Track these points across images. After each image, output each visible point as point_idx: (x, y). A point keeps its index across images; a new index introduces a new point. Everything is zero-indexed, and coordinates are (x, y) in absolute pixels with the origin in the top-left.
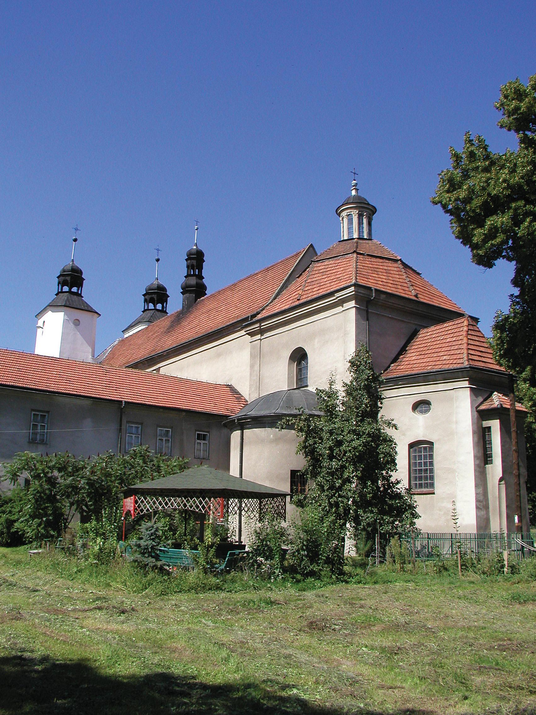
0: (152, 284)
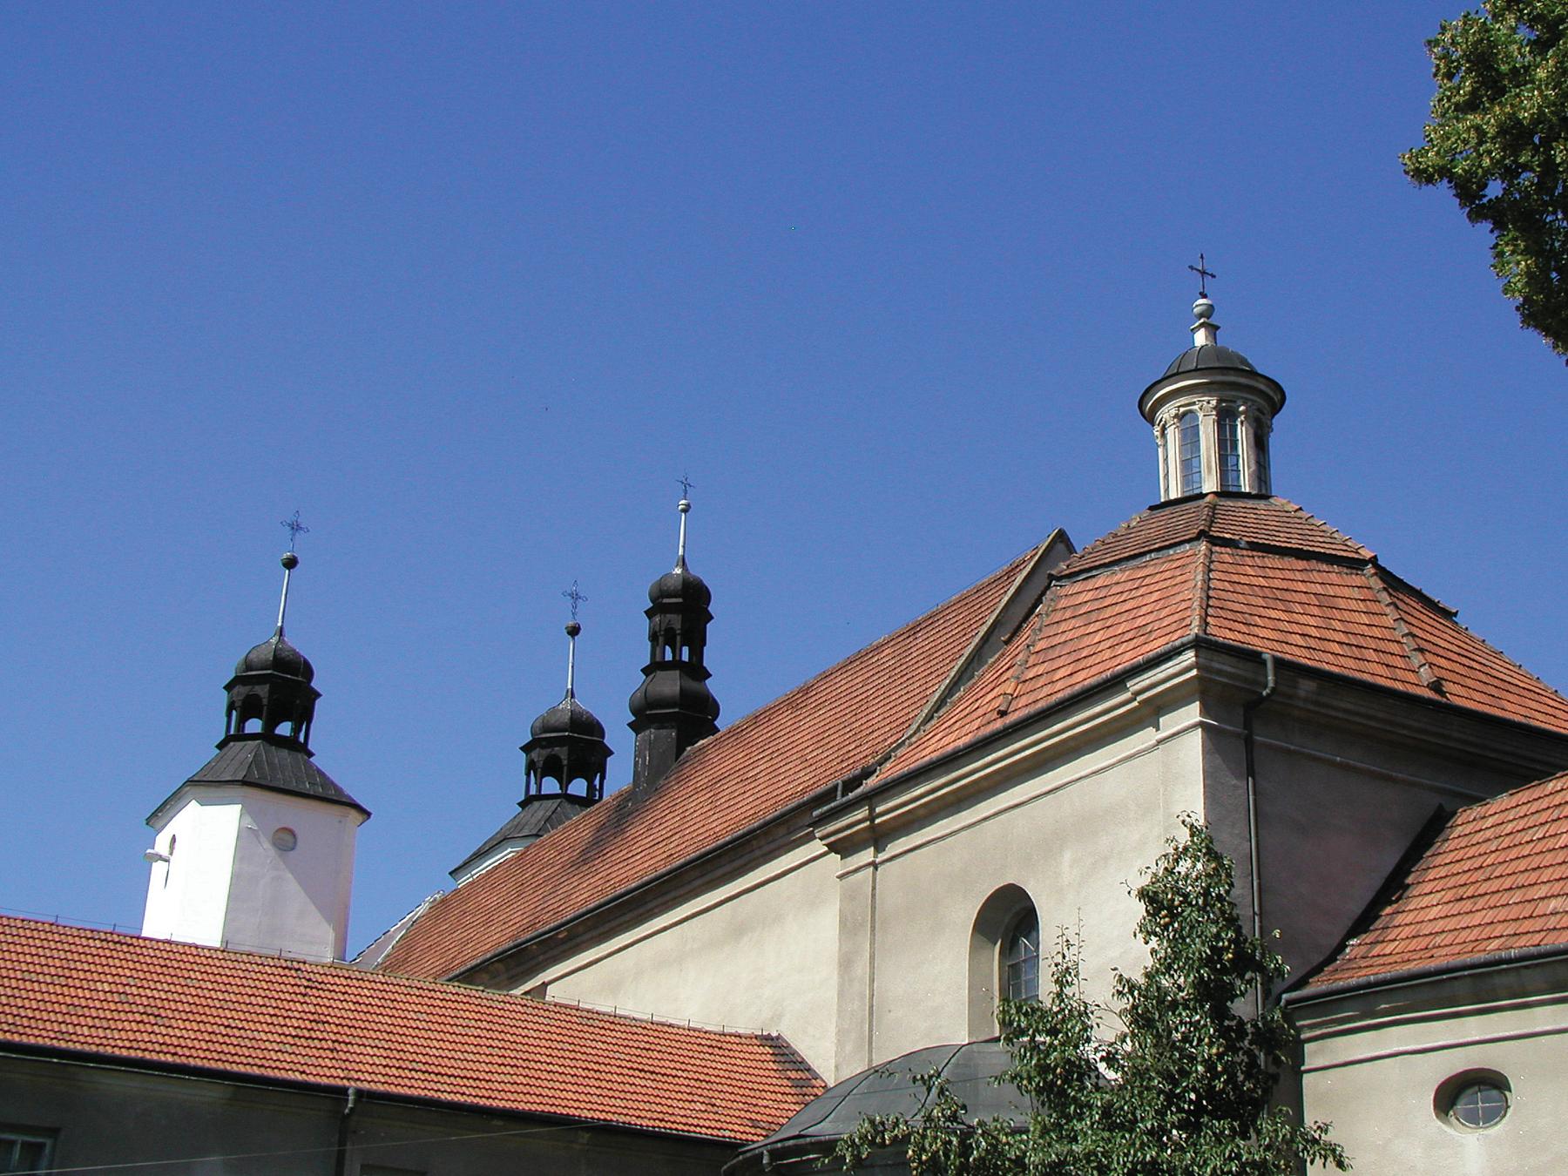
0: (554, 710)
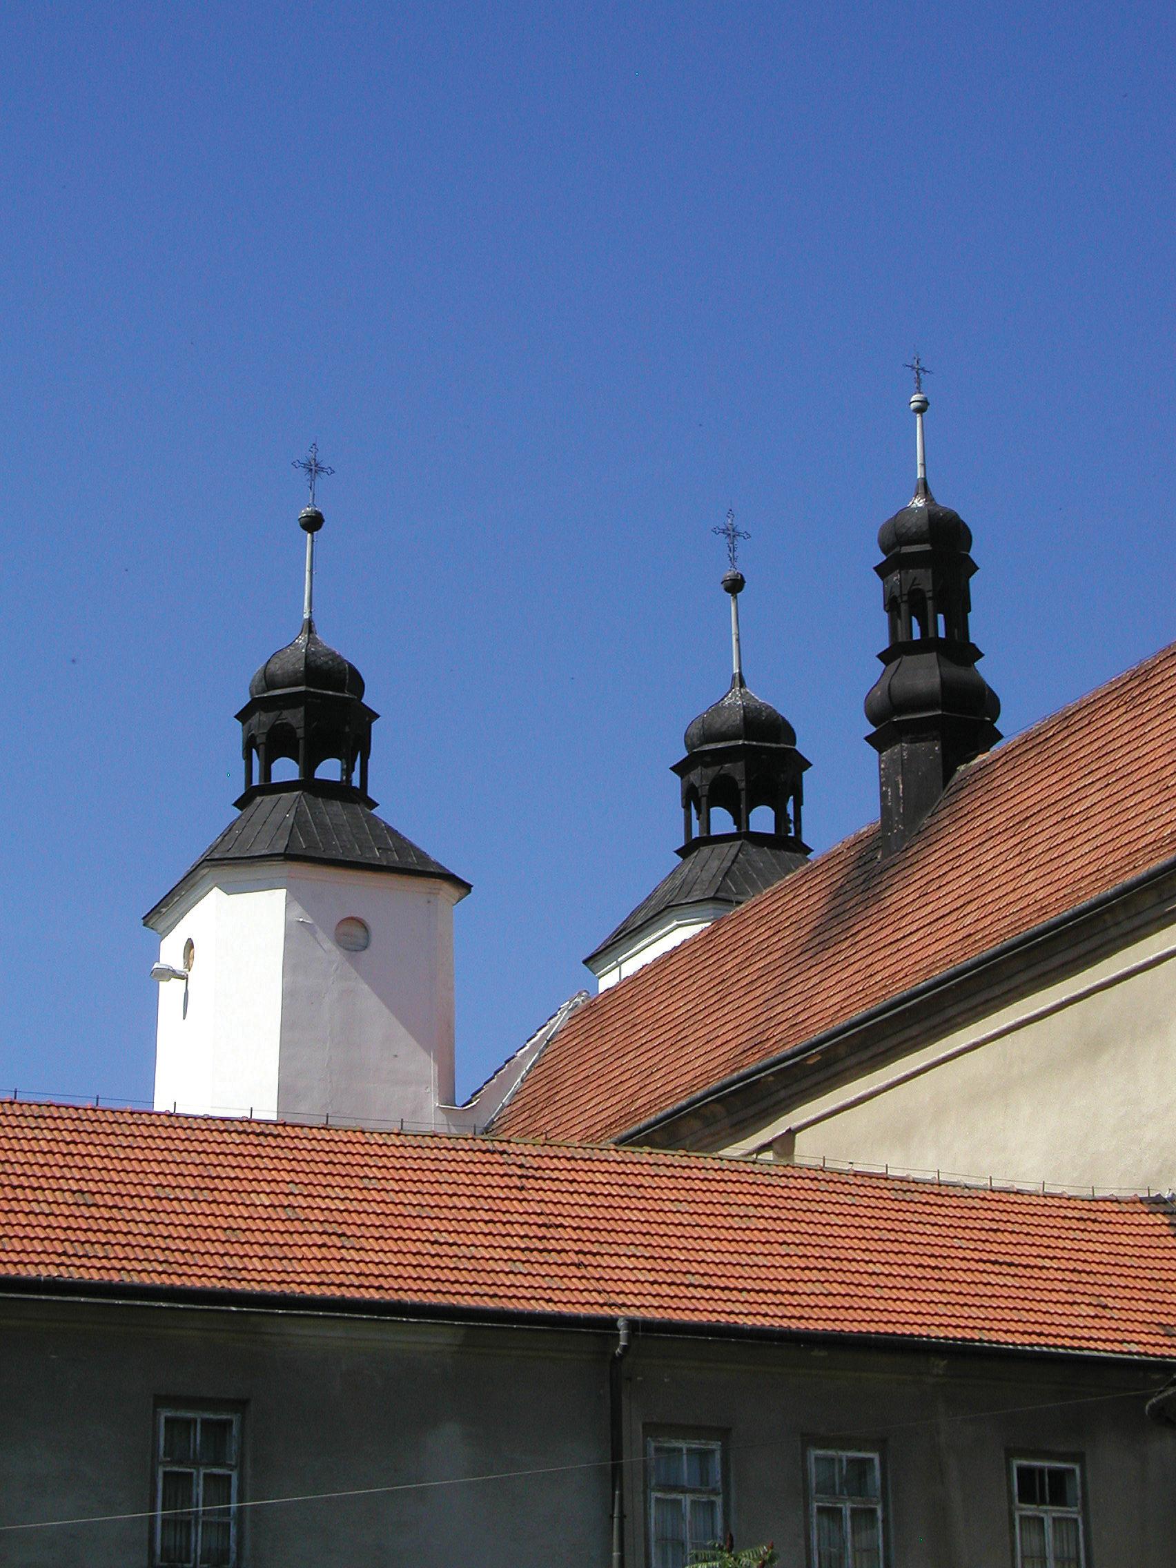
0: (717, 708)
